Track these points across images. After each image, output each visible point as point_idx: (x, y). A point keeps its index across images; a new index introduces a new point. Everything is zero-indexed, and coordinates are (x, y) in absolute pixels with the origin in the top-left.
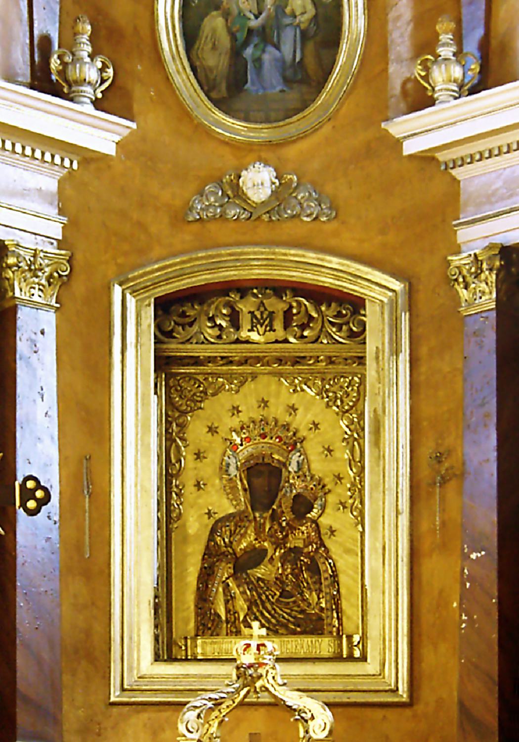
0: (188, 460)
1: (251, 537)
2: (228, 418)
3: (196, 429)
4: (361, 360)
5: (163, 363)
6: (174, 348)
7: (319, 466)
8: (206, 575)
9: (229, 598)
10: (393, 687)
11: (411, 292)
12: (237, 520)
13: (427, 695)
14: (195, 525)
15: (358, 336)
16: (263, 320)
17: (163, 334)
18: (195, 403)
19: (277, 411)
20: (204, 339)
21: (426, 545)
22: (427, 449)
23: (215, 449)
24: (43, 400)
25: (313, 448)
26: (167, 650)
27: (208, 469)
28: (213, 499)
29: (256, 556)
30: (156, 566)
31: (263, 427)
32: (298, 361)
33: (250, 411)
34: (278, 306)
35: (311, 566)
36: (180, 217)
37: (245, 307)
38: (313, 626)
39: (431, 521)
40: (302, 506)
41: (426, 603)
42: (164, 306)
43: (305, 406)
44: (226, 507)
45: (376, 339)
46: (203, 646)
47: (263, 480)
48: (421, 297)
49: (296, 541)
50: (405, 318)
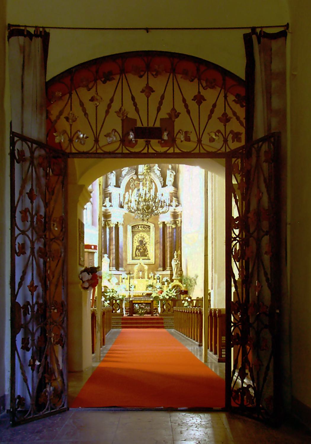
0: (134, 240)
1: (140, 247)
2: (138, 237)
3: (135, 237)
4: (150, 231)
5: (132, 231)
6: (133, 230)
7: (147, 241)
8: (136, 251)
9: (156, 310)
10: (154, 263)
11: (155, 226)
12: (139, 246)
13: (156, 263)
14: (135, 247)
15: (150, 229)
16: (141, 227)
17: (132, 229)
18: (135, 235)
19: (142, 235)
20: (136, 229)
21: (156, 249)
22: (156, 240)
23: (137, 239)
24: (121, 275)
25: (146, 239)
26: (133, 259)
27: (136, 241)
28: (136, 244)
29: (140, 249)
30: (111, 151)
31: (141, 237)
32: (144, 231)
33: (140, 235)
34: (142, 226)
35: (145, 250)
36: (134, 218)
37: (140, 226)
38: (146, 256)
39: (157, 247)
40: (145, 244)
41: (156, 254)
42: (132, 227)
43: (145, 235)
44: (138, 245)
45: (151, 230)
46: (136, 258)
47: (141, 242)
48: (156, 226)
49: (144, 248)
50: (154, 228)
